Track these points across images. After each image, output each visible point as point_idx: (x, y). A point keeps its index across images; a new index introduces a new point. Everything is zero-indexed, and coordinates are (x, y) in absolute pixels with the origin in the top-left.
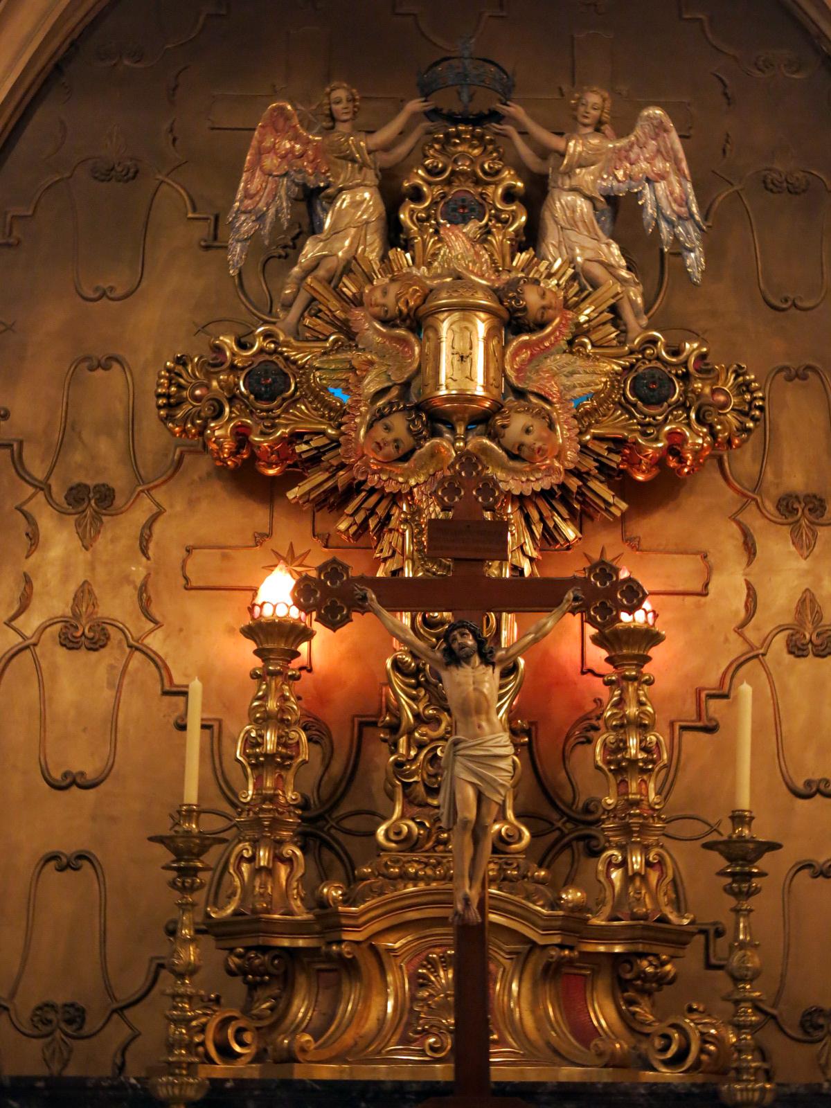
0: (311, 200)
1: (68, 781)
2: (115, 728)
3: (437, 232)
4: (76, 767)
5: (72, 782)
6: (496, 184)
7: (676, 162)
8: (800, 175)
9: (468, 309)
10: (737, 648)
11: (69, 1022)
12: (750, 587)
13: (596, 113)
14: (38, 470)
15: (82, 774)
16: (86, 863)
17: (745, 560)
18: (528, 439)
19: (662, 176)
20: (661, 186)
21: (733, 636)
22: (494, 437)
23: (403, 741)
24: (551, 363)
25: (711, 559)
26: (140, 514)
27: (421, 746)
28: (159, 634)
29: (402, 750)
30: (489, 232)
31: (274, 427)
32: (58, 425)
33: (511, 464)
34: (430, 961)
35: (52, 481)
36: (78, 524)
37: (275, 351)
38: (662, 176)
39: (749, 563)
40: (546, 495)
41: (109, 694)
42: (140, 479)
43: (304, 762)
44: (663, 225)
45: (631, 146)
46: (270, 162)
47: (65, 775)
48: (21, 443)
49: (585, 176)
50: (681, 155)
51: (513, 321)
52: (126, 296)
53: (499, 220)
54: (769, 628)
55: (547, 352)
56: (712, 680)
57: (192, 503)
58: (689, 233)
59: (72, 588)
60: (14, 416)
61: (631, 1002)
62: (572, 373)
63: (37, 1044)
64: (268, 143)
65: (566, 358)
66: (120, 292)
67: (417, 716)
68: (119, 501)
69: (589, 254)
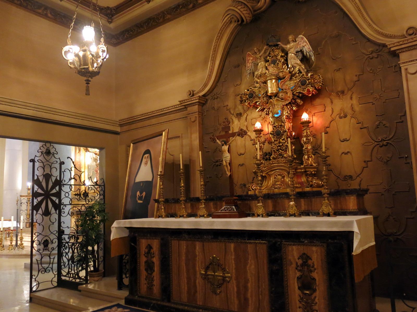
0: (256, 65)
1: (344, 140)
2: (245, 146)
3: (53, 147)
4: (241, 152)
5: (241, 154)
6: (279, 55)
7: (307, 42)
8: (337, 33)
9: (271, 79)
10: (330, 119)
11: (244, 186)
12: (332, 108)
13: (292, 39)
14: (232, 112)
15: (346, 139)
16: (349, 153)
17: (331, 104)
18: (282, 97)
19: (305, 45)
20: (306, 47)
21: (330, 117)
22: (278, 97)
23: (273, 144)
24: (286, 83)
25: (325, 105)
26: (245, 116)
27: (275, 144)
28: (249, 132)
29: (273, 146)
30: (278, 64)
31: (253, 102)
32: (234, 105)
33: (283, 101)
34: (276, 175)
35: (234, 114)
36: (238, 119)
37: (252, 91)
38: (305, 45)
39: (332, 104)
40: (290, 103)
41: (244, 142)
42: (245, 111)
43: (312, 142)
44: (307, 53)
45: (299, 42)
46: (250, 61)
47: (343, 139)
48: (230, 109)
49: (292, 50)
50: (307, 41)
51: (278, 78)
52: (240, 84)
53: (280, 61)
54: (336, 115)
55: (286, 81)
56: (327, 125)
57: (251, 113)
58: (312, 53)
59: (238, 128)
60: (229, 105)
61: (308, 178)
62: (290, 84)
63: (241, 189)
64: (249, 58)
65: (289, 82)
66: (239, 84)
67: (274, 140)
68: (242, 114)
69: (294, 63)
